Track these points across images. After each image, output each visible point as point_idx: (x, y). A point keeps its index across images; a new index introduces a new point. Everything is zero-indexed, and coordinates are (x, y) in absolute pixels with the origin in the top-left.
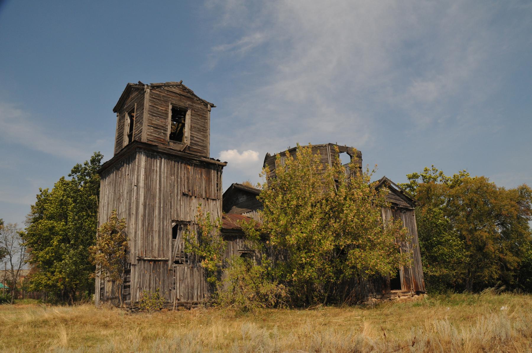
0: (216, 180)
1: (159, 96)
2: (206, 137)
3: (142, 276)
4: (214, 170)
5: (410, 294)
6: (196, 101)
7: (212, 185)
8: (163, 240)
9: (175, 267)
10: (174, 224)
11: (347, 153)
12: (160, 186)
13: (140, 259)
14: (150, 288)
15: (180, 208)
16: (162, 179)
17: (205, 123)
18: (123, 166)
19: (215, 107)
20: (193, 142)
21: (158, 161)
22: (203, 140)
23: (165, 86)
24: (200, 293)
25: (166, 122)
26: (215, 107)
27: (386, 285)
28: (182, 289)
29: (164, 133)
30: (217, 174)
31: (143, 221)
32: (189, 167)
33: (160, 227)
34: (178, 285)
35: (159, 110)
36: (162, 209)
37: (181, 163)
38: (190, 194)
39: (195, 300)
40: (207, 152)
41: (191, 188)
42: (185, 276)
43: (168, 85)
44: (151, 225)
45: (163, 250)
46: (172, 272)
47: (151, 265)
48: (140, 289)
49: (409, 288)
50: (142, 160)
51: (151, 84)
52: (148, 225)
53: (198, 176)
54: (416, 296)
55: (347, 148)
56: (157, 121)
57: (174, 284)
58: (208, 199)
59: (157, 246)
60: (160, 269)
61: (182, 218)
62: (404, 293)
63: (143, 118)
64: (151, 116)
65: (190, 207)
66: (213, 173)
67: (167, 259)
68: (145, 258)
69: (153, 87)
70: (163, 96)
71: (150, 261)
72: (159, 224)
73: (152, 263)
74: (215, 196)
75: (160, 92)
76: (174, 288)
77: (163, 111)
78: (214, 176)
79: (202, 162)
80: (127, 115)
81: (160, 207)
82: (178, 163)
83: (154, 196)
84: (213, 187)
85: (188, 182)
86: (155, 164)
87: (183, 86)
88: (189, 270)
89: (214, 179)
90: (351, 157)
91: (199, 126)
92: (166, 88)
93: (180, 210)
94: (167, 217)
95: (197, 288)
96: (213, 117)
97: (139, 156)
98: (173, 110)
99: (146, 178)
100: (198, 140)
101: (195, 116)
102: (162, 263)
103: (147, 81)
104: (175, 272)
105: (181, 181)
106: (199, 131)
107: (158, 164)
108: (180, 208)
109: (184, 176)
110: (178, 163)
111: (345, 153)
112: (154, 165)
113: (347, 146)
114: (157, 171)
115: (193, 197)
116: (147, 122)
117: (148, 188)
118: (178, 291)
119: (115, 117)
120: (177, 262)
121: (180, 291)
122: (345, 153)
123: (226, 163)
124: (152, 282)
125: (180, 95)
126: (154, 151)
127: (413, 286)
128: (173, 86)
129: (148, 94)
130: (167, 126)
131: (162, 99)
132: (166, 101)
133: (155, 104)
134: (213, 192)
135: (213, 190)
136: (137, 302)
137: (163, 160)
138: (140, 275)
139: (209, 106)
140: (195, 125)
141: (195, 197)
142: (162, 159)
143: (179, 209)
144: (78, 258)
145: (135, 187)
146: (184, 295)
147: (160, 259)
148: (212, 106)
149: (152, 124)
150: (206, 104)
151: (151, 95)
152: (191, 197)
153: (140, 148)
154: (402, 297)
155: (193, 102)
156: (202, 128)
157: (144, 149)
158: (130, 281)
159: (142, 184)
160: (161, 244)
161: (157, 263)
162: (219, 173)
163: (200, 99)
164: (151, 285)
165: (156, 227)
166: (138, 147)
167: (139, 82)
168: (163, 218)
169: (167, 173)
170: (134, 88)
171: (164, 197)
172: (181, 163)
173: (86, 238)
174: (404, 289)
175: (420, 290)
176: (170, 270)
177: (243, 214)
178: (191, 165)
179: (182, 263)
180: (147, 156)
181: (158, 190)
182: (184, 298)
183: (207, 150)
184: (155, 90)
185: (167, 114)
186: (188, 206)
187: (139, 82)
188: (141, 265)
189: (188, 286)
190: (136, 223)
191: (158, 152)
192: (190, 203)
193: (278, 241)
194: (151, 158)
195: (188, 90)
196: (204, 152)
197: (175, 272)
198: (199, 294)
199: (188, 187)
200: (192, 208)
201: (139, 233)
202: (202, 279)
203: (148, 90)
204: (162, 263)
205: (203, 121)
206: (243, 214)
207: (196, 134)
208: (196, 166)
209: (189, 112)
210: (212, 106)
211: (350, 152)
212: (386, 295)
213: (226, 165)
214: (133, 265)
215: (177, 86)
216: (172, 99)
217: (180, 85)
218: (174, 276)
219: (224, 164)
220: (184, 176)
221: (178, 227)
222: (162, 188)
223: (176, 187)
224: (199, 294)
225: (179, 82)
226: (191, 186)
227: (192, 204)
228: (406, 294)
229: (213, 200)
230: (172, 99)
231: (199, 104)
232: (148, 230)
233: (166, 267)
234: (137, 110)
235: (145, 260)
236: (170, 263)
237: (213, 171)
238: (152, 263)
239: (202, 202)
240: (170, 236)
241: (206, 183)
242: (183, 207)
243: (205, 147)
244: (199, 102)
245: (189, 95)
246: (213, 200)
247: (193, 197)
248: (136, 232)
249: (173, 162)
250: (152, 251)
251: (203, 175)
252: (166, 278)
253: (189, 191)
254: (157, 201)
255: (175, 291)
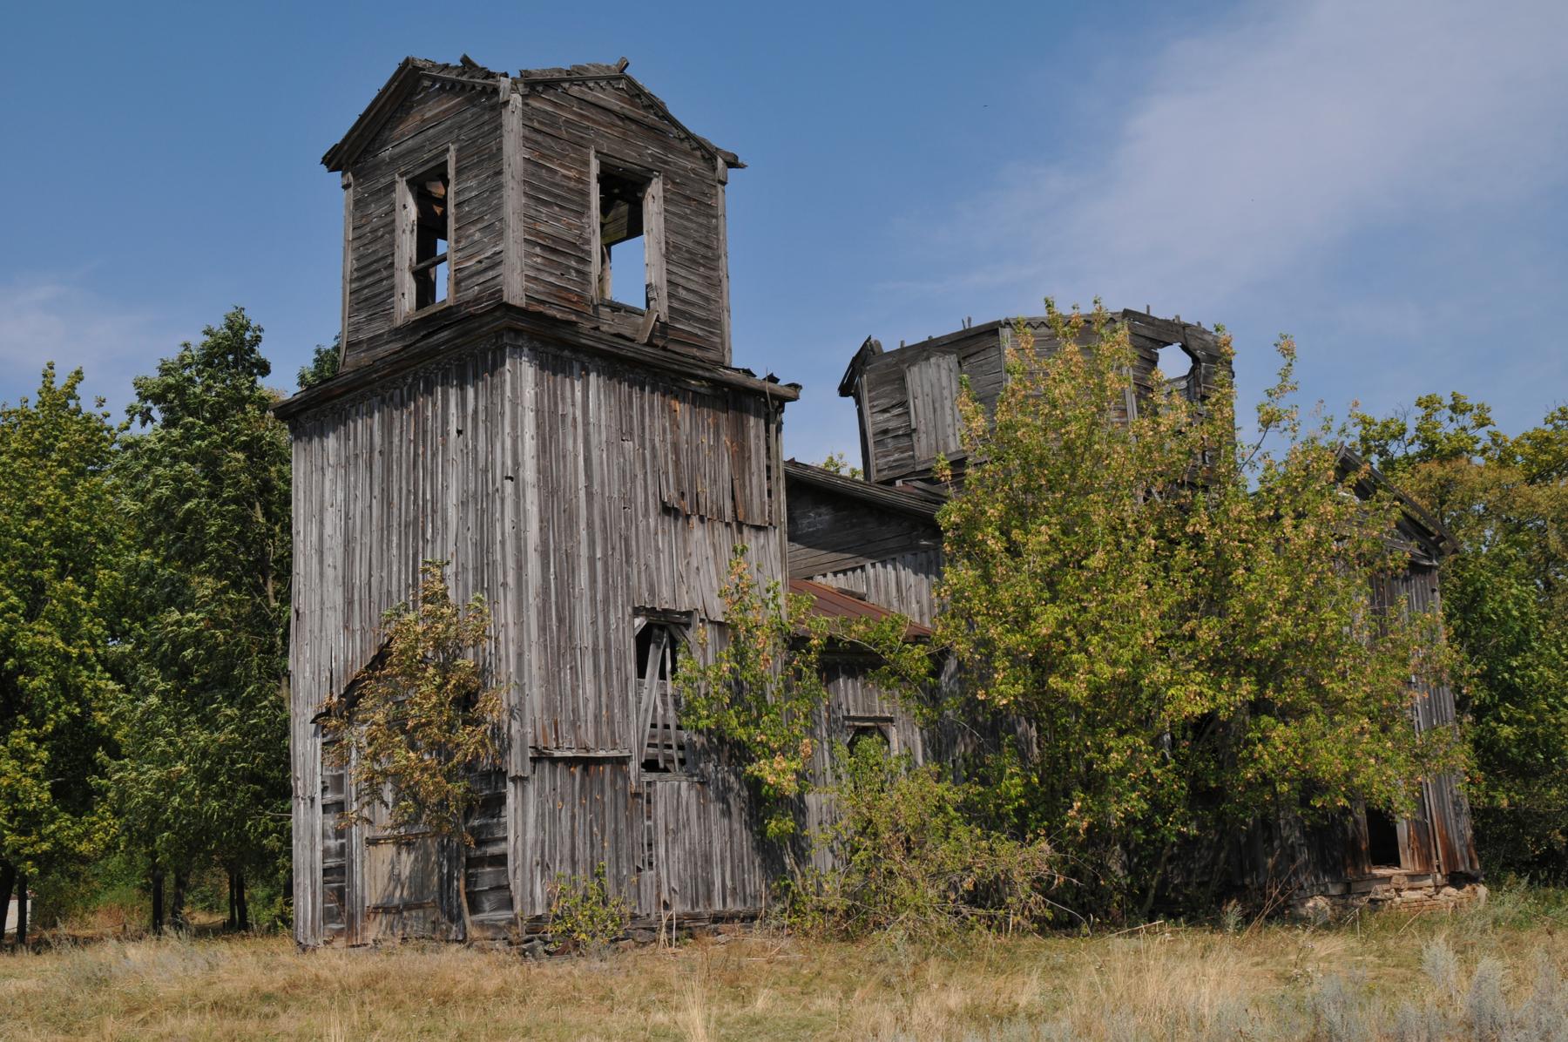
0: (763, 452)
1: (552, 120)
2: (715, 284)
3: (547, 818)
4: (757, 416)
5: (1430, 882)
6: (676, 143)
7: (751, 474)
8: (609, 685)
9: (649, 784)
10: (640, 622)
11: (1185, 348)
12: (589, 476)
13: (540, 758)
14: (574, 863)
15: (658, 558)
16: (595, 454)
17: (708, 229)
18: (429, 391)
20: (676, 305)
21: (578, 385)
22: (707, 299)
23: (571, 82)
25: (582, 228)
27: (1348, 848)
28: (676, 867)
29: (577, 271)
30: (767, 430)
31: (543, 611)
32: (678, 406)
33: (596, 637)
34: (662, 851)
35: (558, 179)
36: (599, 565)
37: (652, 392)
38: (686, 506)
39: (718, 906)
40: (722, 347)
41: (686, 485)
42: (682, 815)
43: (578, 77)
44: (565, 620)
45: (611, 721)
46: (641, 800)
47: (573, 776)
48: (545, 867)
49: (1427, 860)
50: (523, 377)
51: (525, 74)
52: (559, 628)
53: (706, 440)
54: (1451, 890)
55: (1185, 326)
56: (555, 225)
57: (650, 845)
58: (740, 525)
59: (591, 705)
60: (602, 792)
61: (664, 601)
62: (1412, 877)
63: (499, 207)
64: (532, 203)
65: (688, 555)
66: (754, 425)
67: (626, 754)
68: (557, 754)
69: (534, 85)
70: (567, 121)
71: (570, 762)
72: (594, 623)
73: (577, 771)
74: (763, 512)
75: (555, 104)
76: (651, 864)
77: (572, 184)
78: (758, 437)
79: (717, 384)
80: (402, 187)
81: (592, 560)
82: (642, 390)
83: (570, 518)
84: (755, 480)
85: (677, 463)
86: (568, 394)
87: (631, 82)
88: (693, 793)
89: (758, 451)
90: (1196, 360)
91: (690, 244)
92: (575, 90)
93: (658, 569)
94: (616, 596)
95: (723, 861)
96: (737, 199)
97: (514, 365)
98: (607, 179)
99: (543, 449)
100: (690, 297)
101: (676, 204)
102: (608, 768)
103: (507, 56)
104: (649, 802)
105: (654, 456)
106: (692, 261)
107: (578, 394)
108: (658, 558)
109: (664, 440)
110: (642, 390)
111: (1177, 346)
112: (563, 398)
113: (1184, 319)
114: (574, 419)
115: (694, 520)
116: (521, 227)
117: (550, 487)
118: (664, 874)
119: (334, 191)
120: (650, 765)
121: (670, 867)
122: (1177, 346)
123: (796, 387)
125: (625, 118)
126: (563, 344)
127: (1439, 857)
128: (596, 80)
129: (518, 113)
130: (588, 242)
131: (565, 135)
132: (579, 144)
133: (543, 156)
134: (756, 501)
135: (755, 491)
136: (539, 918)
137: (593, 377)
138: (540, 816)
139: (720, 161)
140: (679, 240)
141: (702, 519)
142: (588, 374)
143: (653, 567)
145: (509, 485)
146: (683, 887)
147: (601, 754)
148: (733, 163)
149: (538, 233)
150: (709, 155)
151: (528, 116)
152: (688, 517)
153: (518, 332)
154: (1407, 894)
155: (668, 148)
156: (702, 251)
157: (532, 337)
158: (505, 839)
159: (529, 473)
160: (604, 699)
161: (592, 769)
162: (773, 427)
163: (690, 136)
164: (579, 855)
165: (585, 638)
166: (510, 329)
167: (466, 60)
168: (606, 601)
169: (608, 427)
170: (435, 80)
171: (604, 520)
172: (652, 392)
173: (1278, 743)
174: (1409, 864)
175: (1462, 869)
176: (637, 795)
177: (819, 579)
178: (681, 395)
179: (666, 770)
180: (542, 367)
181: (582, 494)
182: (683, 900)
183: (721, 336)
184: (538, 96)
185: (585, 194)
186: (681, 552)
187: (466, 60)
188: (542, 780)
189: (692, 852)
190: (520, 623)
191: (577, 348)
192: (685, 541)
194: (555, 374)
195: (649, 96)
196: (714, 346)
197: (649, 802)
198: (729, 883)
199: (678, 482)
200: (694, 564)
201: (534, 657)
203: (516, 99)
204: (608, 768)
205: (702, 220)
206: (819, 579)
207: (683, 273)
208: (697, 400)
209: (656, 189)
210: (733, 163)
211: (1193, 344)
212: (1361, 887)
213: (795, 399)
214: (514, 779)
215: (609, 79)
216: (597, 133)
217: (618, 78)
218: (649, 818)
219: (790, 392)
220: (664, 440)
221: (661, 631)
222: (596, 487)
223: (639, 482)
224: (729, 883)
225: (611, 61)
226: (685, 475)
227: (691, 548)
228: (1417, 884)
229: (759, 528)
230: (597, 133)
231: (687, 154)
232: (560, 649)
233: (620, 782)
234: (459, 172)
235: (554, 761)
236: (634, 767)
237: (752, 420)
238: (577, 771)
239: (724, 536)
240: (632, 667)
241: (733, 465)
242: (665, 557)
243: (714, 324)
244: (686, 146)
245: (649, 116)
246: (759, 528)
247: (694, 520)
248: (520, 655)
249: (625, 387)
250: (574, 726)
251: (724, 438)
252: (622, 826)
253: (683, 495)
254: (583, 533)
255: (653, 873)
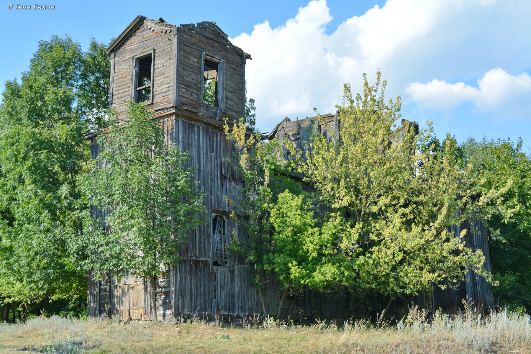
19: (251, 59)
24: (241, 303)
26: (251, 59)
29: (196, 94)
57: (215, 291)
88: (229, 273)
124: (193, 288)
144: (233, 198)
189: (228, 294)
193: (310, 258)
198: (240, 305)
202: (243, 285)
224: (240, 305)
233: (206, 269)
